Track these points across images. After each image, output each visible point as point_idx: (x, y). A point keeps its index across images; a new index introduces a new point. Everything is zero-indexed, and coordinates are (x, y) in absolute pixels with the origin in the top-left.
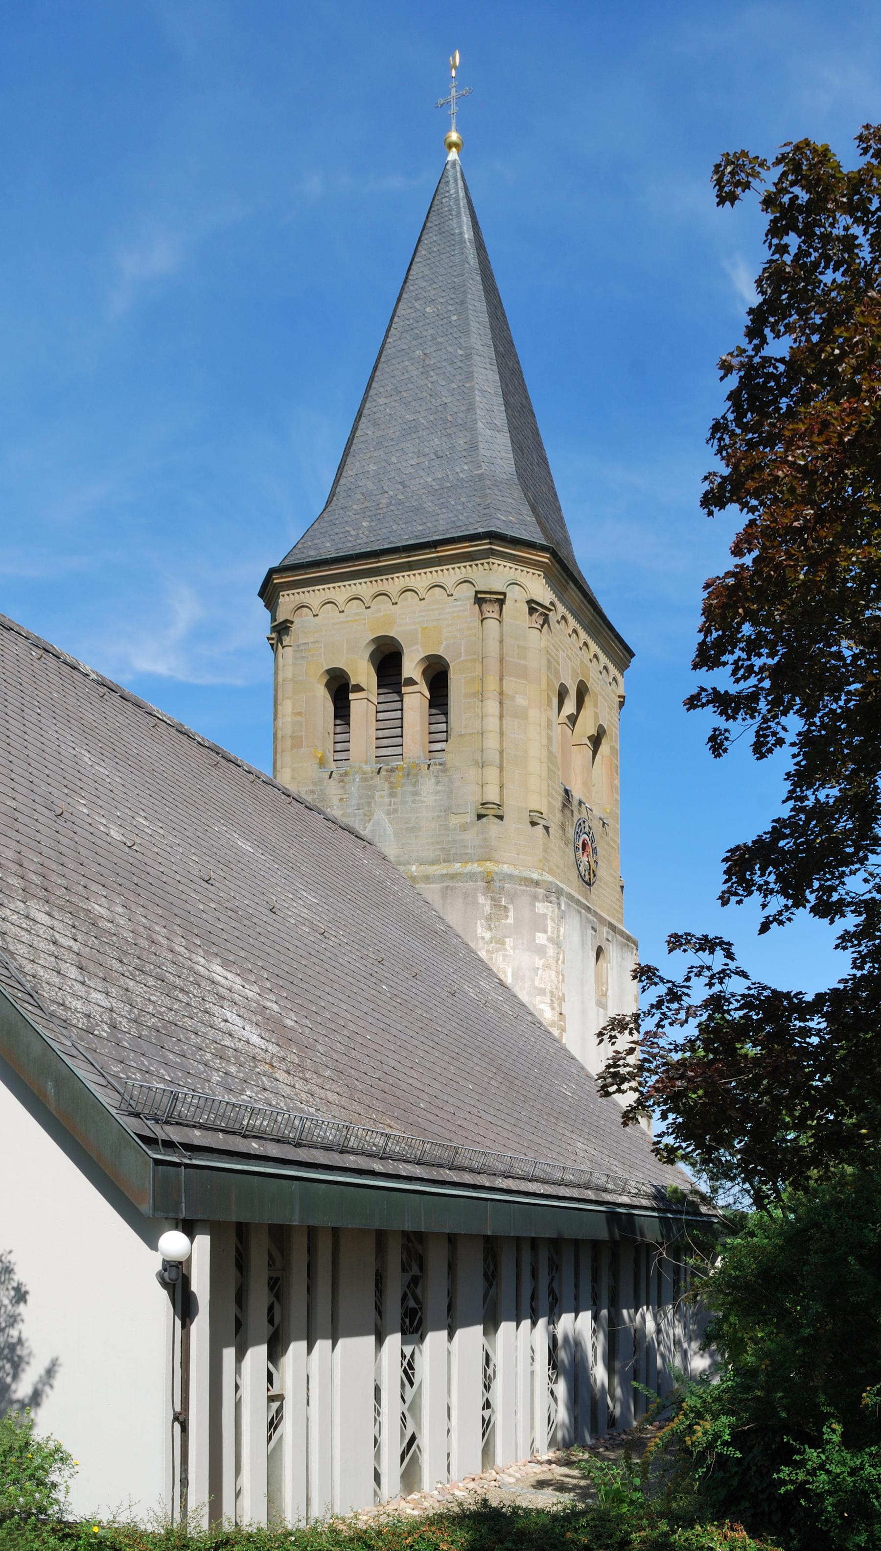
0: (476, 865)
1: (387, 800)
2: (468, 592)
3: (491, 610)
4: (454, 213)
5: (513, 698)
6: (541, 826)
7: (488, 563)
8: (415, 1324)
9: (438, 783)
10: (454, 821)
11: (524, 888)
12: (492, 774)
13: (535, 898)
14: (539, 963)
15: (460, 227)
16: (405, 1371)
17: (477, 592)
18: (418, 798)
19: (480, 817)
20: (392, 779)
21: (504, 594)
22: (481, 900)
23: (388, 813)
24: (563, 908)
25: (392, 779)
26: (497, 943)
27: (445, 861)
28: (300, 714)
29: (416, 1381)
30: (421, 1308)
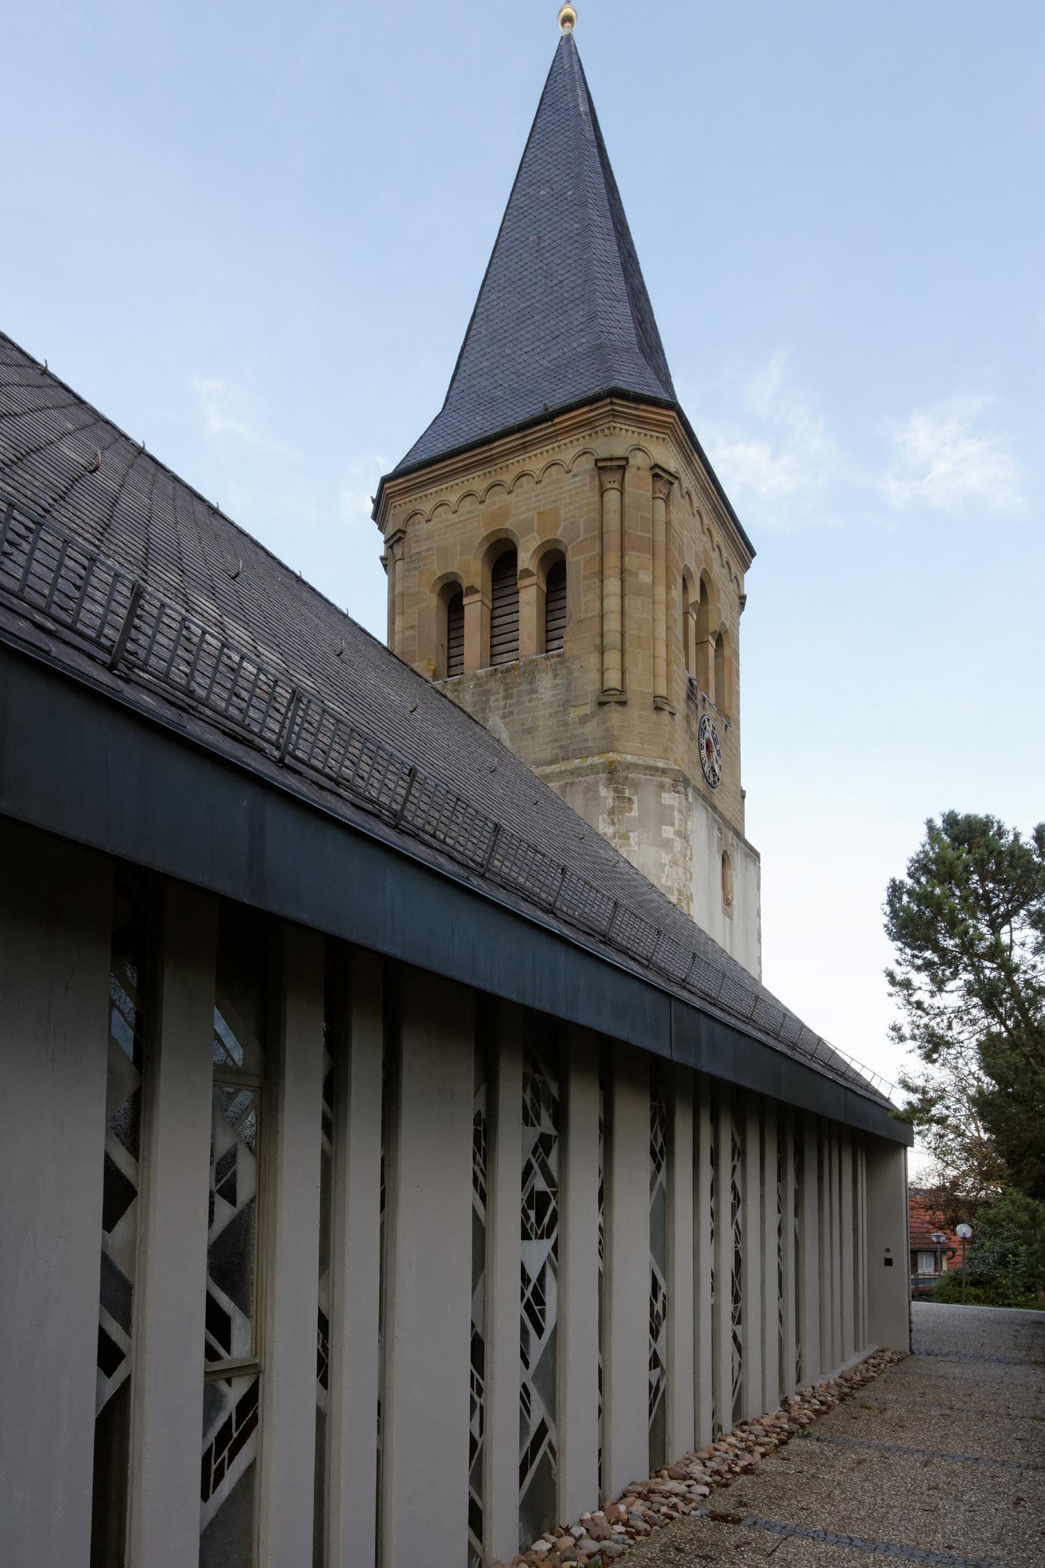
0: (596, 758)
1: (502, 703)
2: (587, 464)
3: (611, 480)
4: (568, 87)
5: (635, 575)
6: (666, 713)
7: (609, 428)
8: (546, 1220)
9: (555, 676)
10: (574, 714)
11: (649, 777)
12: (613, 658)
13: (661, 787)
14: (666, 858)
15: (576, 100)
16: (528, 1307)
17: (597, 461)
18: (534, 696)
19: (602, 704)
20: (508, 680)
21: (626, 459)
22: (603, 792)
23: (504, 717)
24: (690, 800)
25: (508, 680)
26: (620, 838)
27: (563, 759)
28: (412, 627)
29: (548, 1326)
30: (555, 1193)
